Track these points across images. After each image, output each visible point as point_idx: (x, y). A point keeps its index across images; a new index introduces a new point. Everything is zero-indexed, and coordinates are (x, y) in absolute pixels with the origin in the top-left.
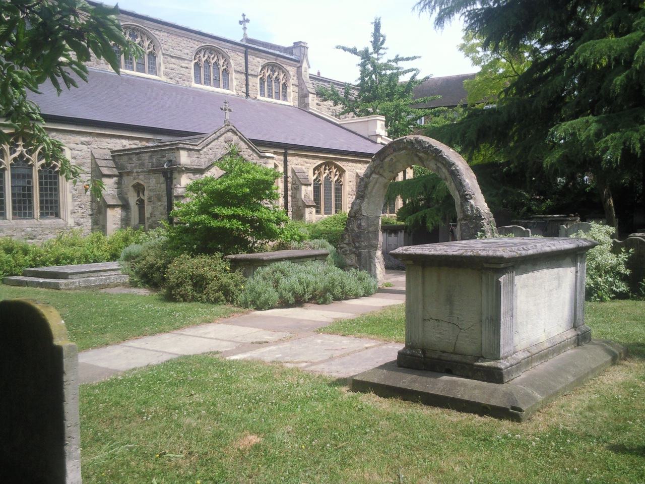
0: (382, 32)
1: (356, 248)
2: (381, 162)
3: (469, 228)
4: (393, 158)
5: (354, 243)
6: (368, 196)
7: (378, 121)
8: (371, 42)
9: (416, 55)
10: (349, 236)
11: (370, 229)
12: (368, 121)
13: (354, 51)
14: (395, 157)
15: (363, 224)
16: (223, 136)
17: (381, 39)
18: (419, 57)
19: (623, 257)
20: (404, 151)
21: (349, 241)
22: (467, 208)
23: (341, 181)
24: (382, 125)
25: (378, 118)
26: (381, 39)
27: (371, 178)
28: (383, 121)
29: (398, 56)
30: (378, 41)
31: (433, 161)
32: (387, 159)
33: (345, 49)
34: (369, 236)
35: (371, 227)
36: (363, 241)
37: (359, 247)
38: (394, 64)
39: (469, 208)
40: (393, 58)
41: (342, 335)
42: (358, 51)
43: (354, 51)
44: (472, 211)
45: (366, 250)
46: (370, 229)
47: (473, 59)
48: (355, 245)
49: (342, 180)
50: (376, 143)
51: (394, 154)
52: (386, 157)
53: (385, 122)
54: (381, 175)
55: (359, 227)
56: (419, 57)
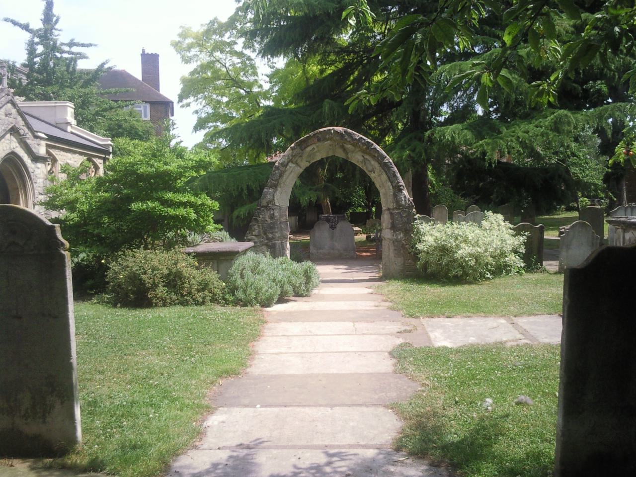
0: (56, 11)
1: (268, 239)
2: (301, 151)
3: (402, 217)
4: (315, 147)
5: (265, 234)
6: (282, 185)
7: (69, 108)
8: (42, 20)
9: (92, 43)
10: (259, 226)
11: (282, 219)
12: (55, 106)
13: (26, 27)
14: (317, 147)
15: (276, 214)
16: (4, 107)
17: (54, 19)
18: (95, 45)
19: (522, 239)
20: (329, 141)
21: (259, 232)
22: (401, 198)
23: (53, 172)
24: (71, 113)
25: (68, 104)
26: (54, 19)
27: (288, 167)
28: (72, 108)
29: (73, 40)
30: (49, 18)
31: (360, 153)
32: (309, 149)
33: (15, 23)
34: (281, 227)
35: (282, 217)
36: (276, 232)
37: (273, 238)
38: (66, 48)
39: (403, 199)
40: (67, 41)
41: (447, 317)
42: (30, 28)
43: (26, 27)
44: (405, 201)
45: (279, 242)
46: (282, 219)
47: (183, 57)
48: (267, 236)
49: (54, 170)
50: (66, 131)
51: (317, 144)
52: (308, 146)
53: (75, 109)
54: (297, 164)
55: (272, 217)
56: (95, 45)
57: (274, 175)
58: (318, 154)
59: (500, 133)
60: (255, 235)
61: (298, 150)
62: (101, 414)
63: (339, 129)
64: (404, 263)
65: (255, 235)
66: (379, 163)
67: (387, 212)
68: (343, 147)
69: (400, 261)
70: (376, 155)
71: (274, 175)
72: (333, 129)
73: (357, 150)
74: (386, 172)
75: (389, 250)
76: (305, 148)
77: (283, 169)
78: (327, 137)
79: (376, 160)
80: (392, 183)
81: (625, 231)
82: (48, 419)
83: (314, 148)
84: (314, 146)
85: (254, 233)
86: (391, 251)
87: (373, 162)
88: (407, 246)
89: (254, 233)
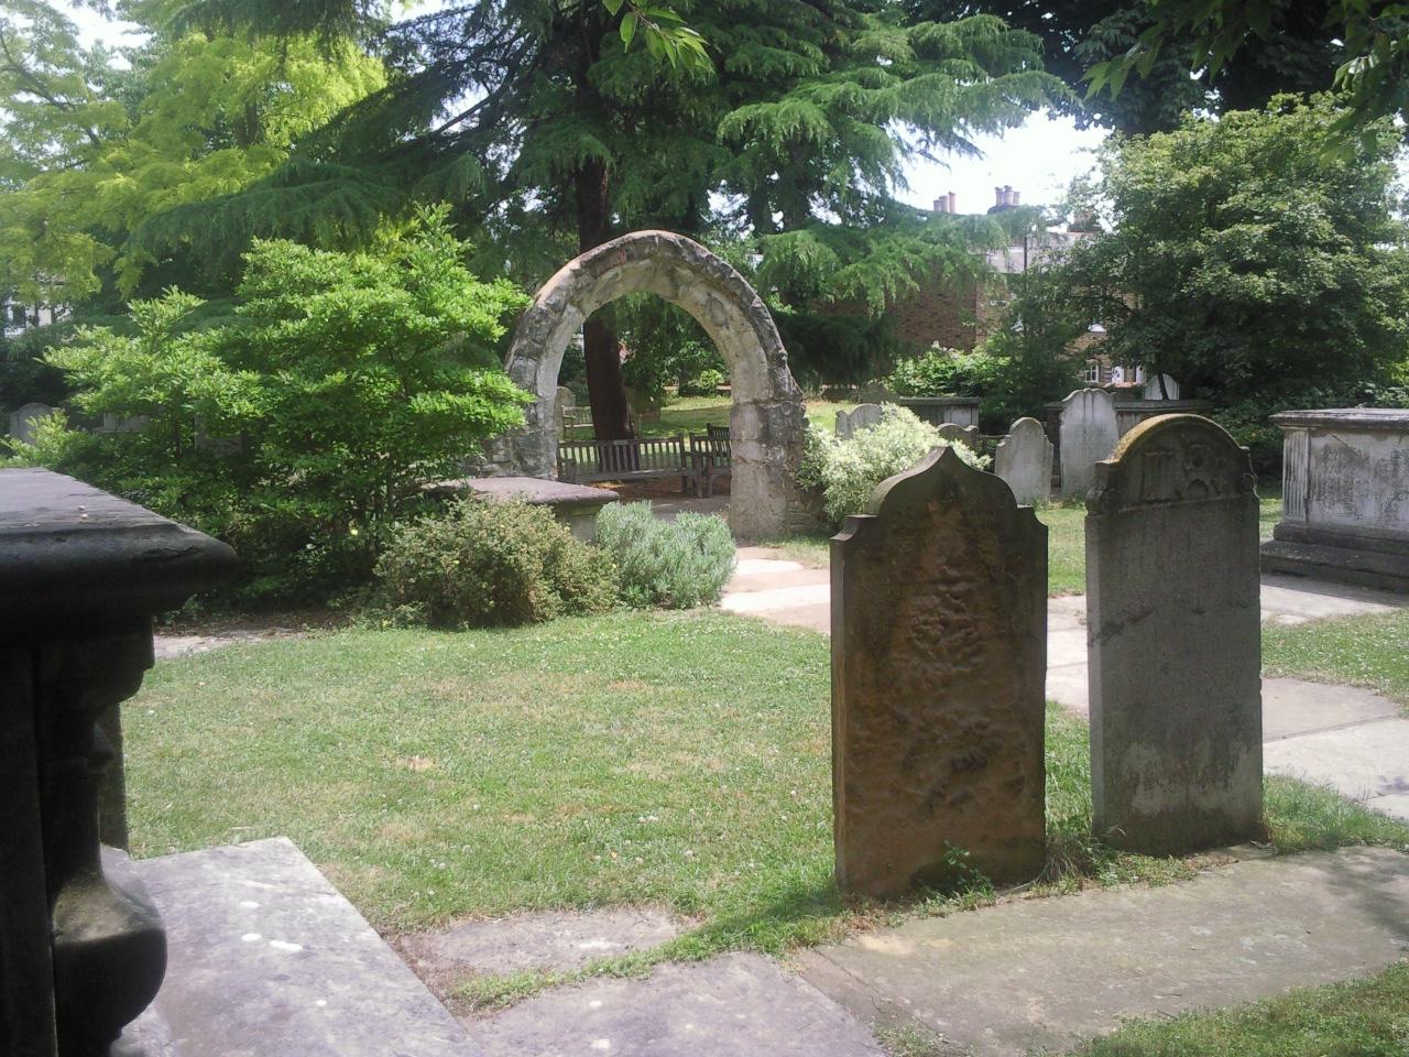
3: (783, 416)
5: (520, 458)
14: (624, 271)
15: (541, 416)
20: (647, 261)
31: (703, 288)
32: (610, 274)
52: (607, 270)
57: (538, 329)
58: (621, 285)
59: (868, 251)
60: (498, 463)
61: (586, 279)
62: (568, 842)
63: (670, 236)
64: (788, 506)
65: (498, 463)
66: (741, 309)
67: (752, 408)
68: (671, 274)
69: (779, 504)
70: (738, 292)
71: (538, 329)
72: (660, 237)
73: (699, 280)
74: (755, 326)
75: (757, 482)
76: (602, 273)
77: (554, 317)
78: (647, 251)
79: (734, 302)
80: (765, 349)
81: (1312, 434)
82: (1232, 781)
83: (617, 275)
84: (617, 270)
85: (495, 457)
86: (761, 484)
87: (728, 306)
88: (792, 474)
89: (495, 457)
